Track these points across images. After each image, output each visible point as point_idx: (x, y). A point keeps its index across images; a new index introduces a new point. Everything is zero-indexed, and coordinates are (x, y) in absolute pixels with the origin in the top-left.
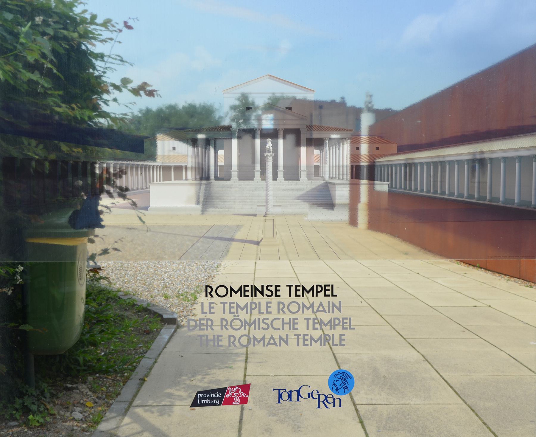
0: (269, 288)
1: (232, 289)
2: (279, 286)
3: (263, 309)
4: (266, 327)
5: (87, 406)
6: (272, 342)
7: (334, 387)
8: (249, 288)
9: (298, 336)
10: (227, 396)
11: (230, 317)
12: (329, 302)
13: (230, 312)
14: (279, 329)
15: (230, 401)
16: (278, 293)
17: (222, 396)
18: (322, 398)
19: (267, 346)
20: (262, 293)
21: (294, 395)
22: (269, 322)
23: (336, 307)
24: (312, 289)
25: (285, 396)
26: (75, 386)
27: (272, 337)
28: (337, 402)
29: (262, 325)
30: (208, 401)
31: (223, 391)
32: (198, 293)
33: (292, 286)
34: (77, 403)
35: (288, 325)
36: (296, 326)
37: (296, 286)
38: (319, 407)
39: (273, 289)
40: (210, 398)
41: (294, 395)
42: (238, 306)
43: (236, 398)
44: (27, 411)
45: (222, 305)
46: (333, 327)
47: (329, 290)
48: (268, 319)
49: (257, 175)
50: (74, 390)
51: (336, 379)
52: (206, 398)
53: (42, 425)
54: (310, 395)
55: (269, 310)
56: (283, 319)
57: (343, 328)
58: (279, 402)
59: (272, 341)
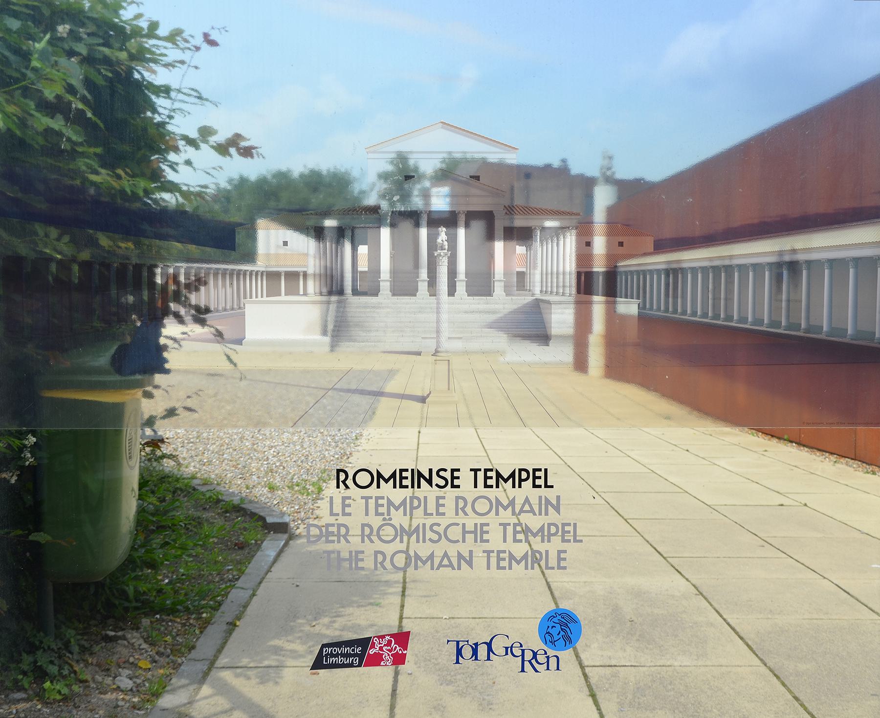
0: (442, 473)
1: (380, 475)
2: (458, 470)
3: (432, 508)
4: (435, 537)
5: (141, 668)
6: (446, 562)
7: (548, 637)
8: (408, 474)
10: (372, 652)
12: (540, 497)
13: (377, 514)
14: (458, 541)
15: (376, 660)
16: (456, 482)
17: (364, 651)
18: (528, 655)
19: (438, 569)
21: (482, 651)
22: (441, 530)
24: (512, 475)
25: (467, 652)
26: (120, 633)
27: (446, 555)
28: (553, 661)
29: (429, 535)
30: (339, 660)
31: (365, 643)
32: (324, 481)
33: (480, 470)
34: (124, 662)
35: (472, 535)
36: (485, 537)
37: (486, 470)
38: (523, 670)
40: (343, 655)
41: (482, 651)
42: (389, 503)
44: (41, 675)
47: (540, 478)
48: (439, 525)
49: (423, 287)
50: (119, 642)
51: (551, 624)
52: (337, 655)
53: (65, 699)
54: (508, 650)
55: (441, 510)
56: (464, 525)
57: (564, 541)
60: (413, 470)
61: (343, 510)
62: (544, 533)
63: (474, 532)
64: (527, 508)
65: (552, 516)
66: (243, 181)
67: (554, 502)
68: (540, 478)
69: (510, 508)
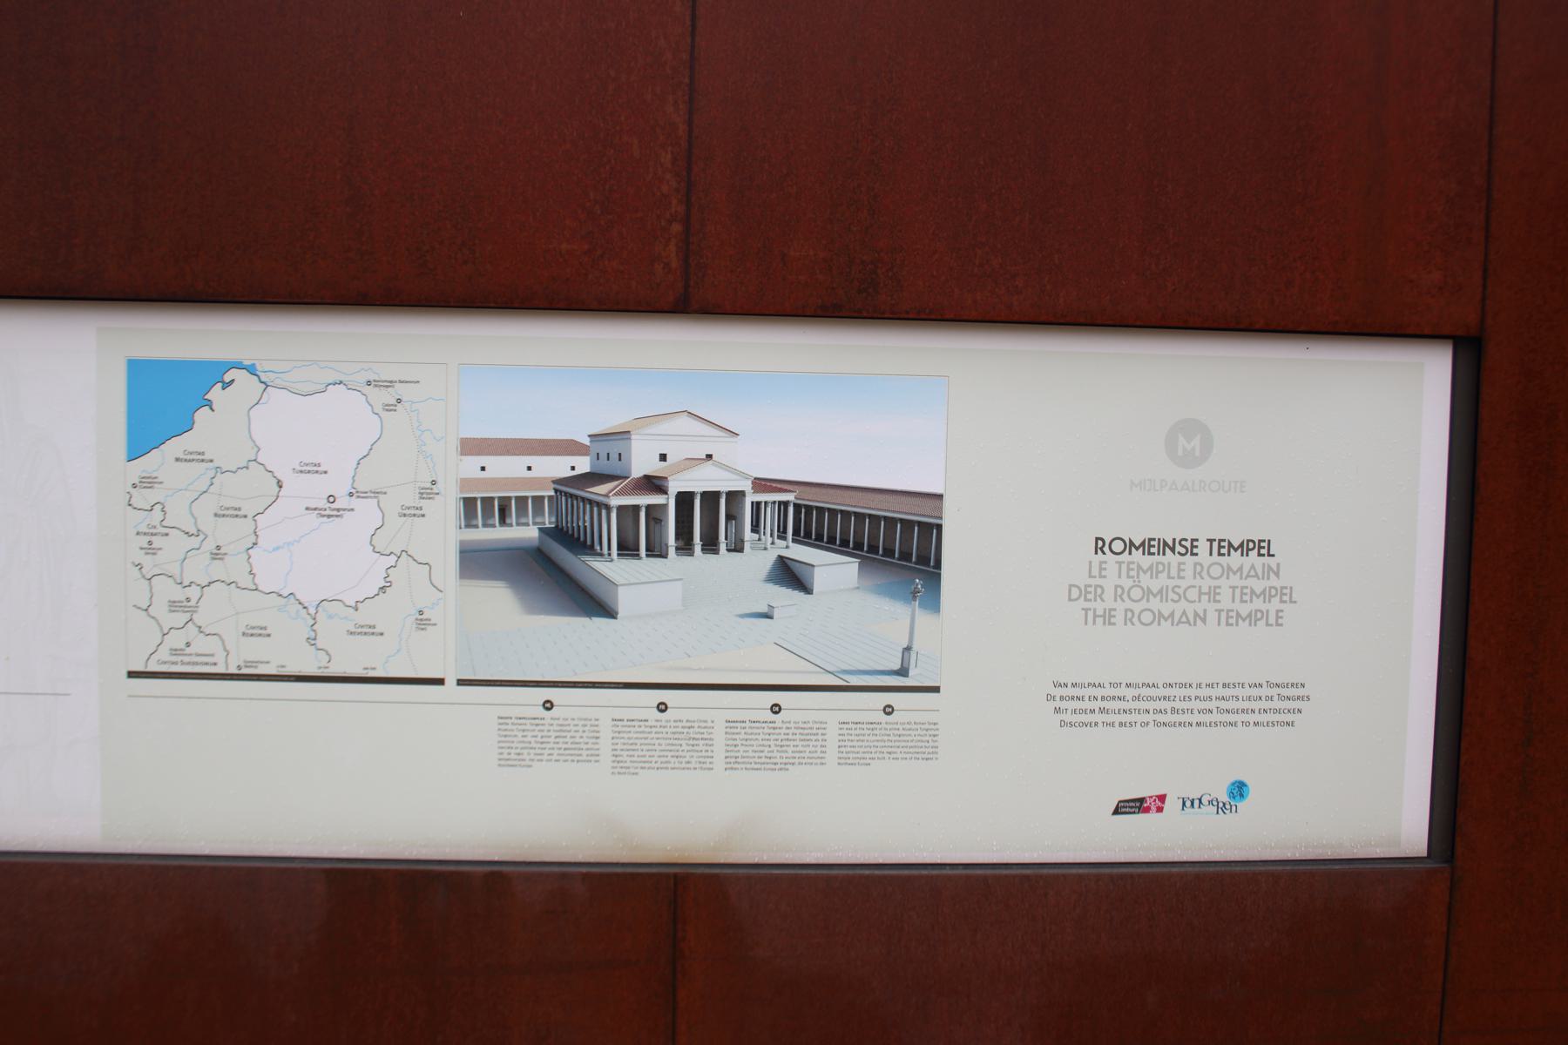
0: (1183, 543)
2: (1197, 540)
3: (1174, 572)
7: (1232, 795)
8: (1155, 543)
9: (1219, 611)
10: (1145, 805)
11: (1127, 583)
12: (1264, 564)
13: (1128, 577)
14: (1195, 601)
15: (1147, 810)
16: (1195, 551)
18: (1221, 805)
19: (1177, 625)
20: (1173, 550)
21: (1196, 803)
22: (1181, 591)
23: (1274, 572)
24: (1241, 545)
25: (1188, 804)
27: (1184, 613)
28: (1234, 808)
29: (1171, 595)
30: (1128, 810)
31: (1142, 800)
33: (1215, 540)
36: (1218, 598)
37: (1220, 541)
38: (1218, 813)
39: (1188, 544)
40: (1129, 807)
41: (1196, 803)
42: (1139, 567)
43: (1153, 808)
45: (1083, 612)
46: (1267, 600)
48: (1179, 587)
52: (1126, 807)
54: (1210, 802)
55: (1280, 621)
56: (1200, 587)
57: (1282, 601)
58: (1183, 809)
60: (1159, 539)
61: (1100, 573)
62: (1266, 595)
63: (1209, 593)
65: (1274, 581)
67: (1275, 569)
69: (1240, 550)
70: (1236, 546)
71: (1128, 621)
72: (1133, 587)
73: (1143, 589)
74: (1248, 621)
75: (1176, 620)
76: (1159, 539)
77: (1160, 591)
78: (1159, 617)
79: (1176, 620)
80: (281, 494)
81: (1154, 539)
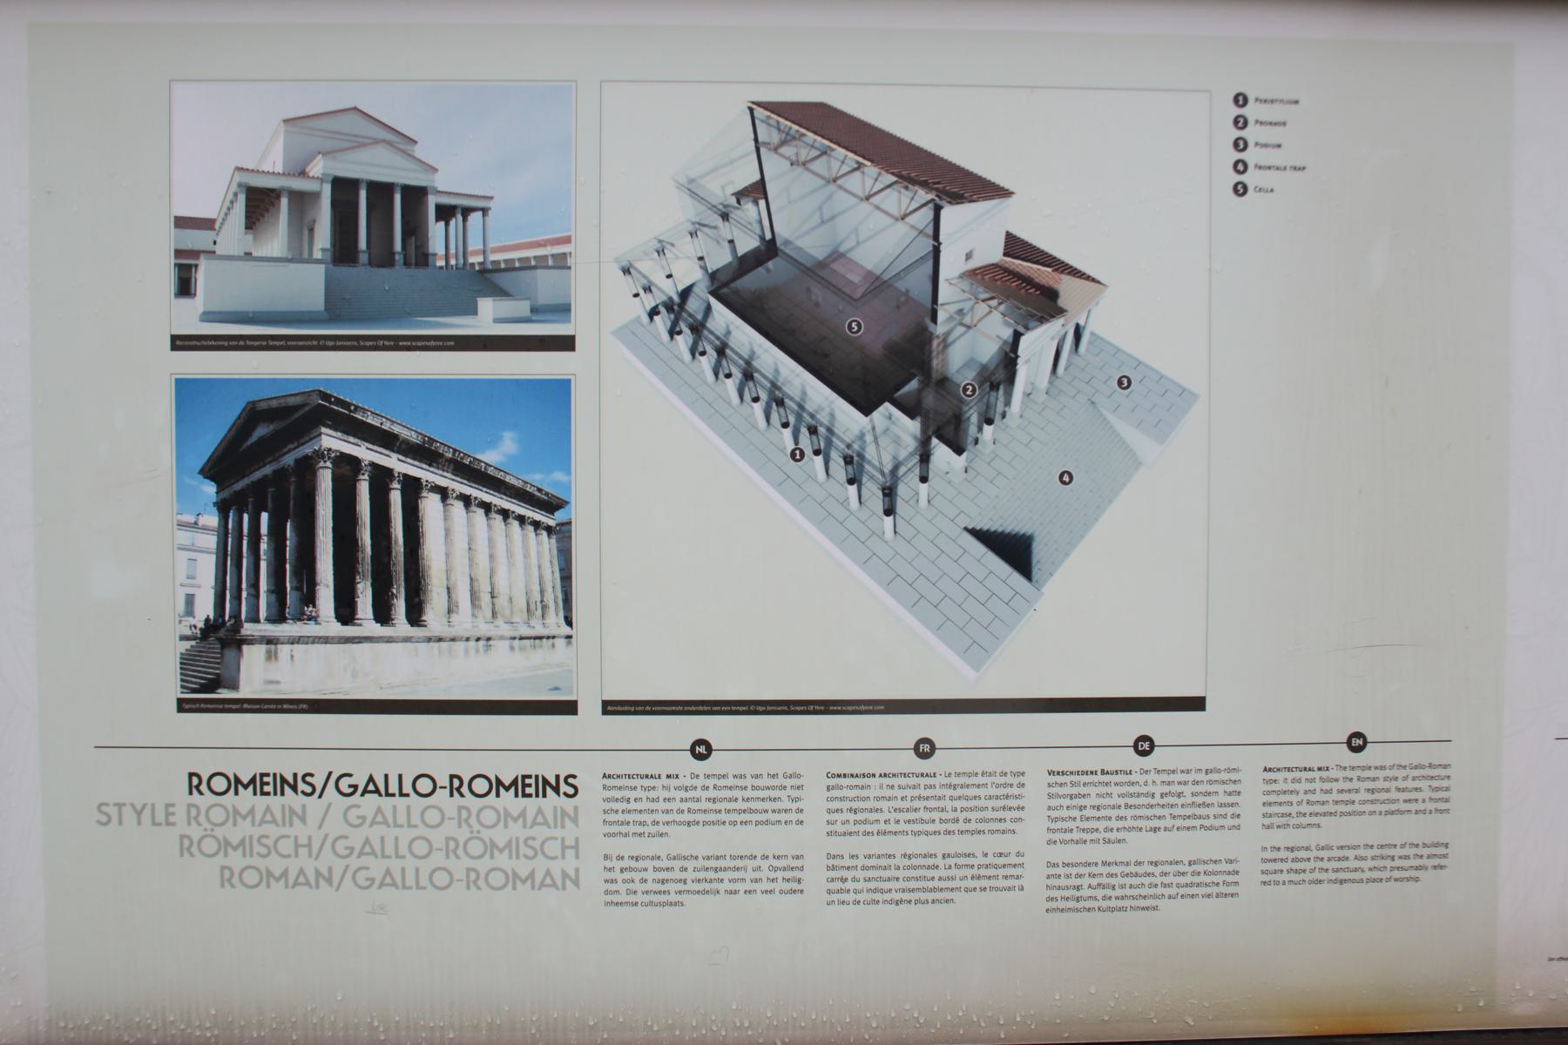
1: (499, 782)
4: (264, 851)
8: (269, 779)
12: (283, 806)
14: (556, 858)
22: (537, 844)
35: (573, 851)
47: (530, 785)
48: (534, 839)
55: (172, 819)
59: (301, 880)
61: (167, 819)
64: (268, 817)
66: (248, 485)
68: (530, 785)
69: (513, 788)
70: (507, 783)
71: (472, 885)
72: (471, 839)
73: (218, 840)
74: (240, 850)
75: (291, 882)
76: (537, 777)
77: (242, 842)
78: (514, 878)
79: (291, 882)
80: (818, 214)
81: (530, 777)
